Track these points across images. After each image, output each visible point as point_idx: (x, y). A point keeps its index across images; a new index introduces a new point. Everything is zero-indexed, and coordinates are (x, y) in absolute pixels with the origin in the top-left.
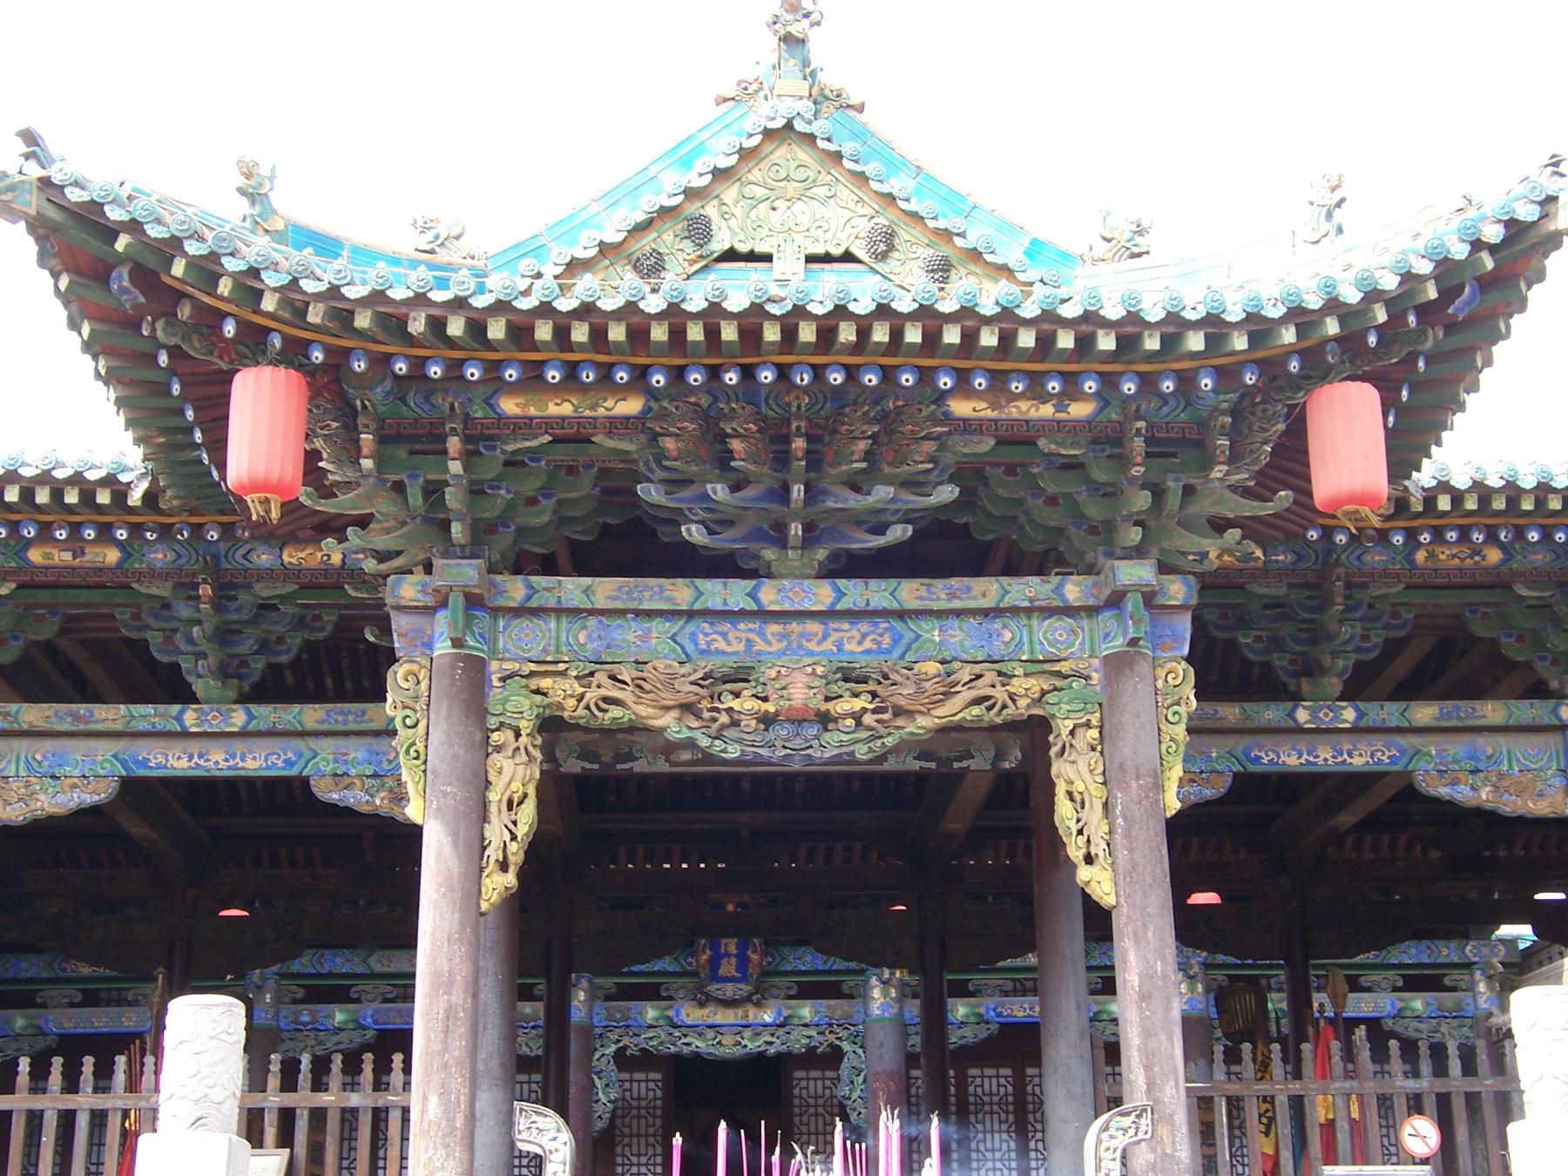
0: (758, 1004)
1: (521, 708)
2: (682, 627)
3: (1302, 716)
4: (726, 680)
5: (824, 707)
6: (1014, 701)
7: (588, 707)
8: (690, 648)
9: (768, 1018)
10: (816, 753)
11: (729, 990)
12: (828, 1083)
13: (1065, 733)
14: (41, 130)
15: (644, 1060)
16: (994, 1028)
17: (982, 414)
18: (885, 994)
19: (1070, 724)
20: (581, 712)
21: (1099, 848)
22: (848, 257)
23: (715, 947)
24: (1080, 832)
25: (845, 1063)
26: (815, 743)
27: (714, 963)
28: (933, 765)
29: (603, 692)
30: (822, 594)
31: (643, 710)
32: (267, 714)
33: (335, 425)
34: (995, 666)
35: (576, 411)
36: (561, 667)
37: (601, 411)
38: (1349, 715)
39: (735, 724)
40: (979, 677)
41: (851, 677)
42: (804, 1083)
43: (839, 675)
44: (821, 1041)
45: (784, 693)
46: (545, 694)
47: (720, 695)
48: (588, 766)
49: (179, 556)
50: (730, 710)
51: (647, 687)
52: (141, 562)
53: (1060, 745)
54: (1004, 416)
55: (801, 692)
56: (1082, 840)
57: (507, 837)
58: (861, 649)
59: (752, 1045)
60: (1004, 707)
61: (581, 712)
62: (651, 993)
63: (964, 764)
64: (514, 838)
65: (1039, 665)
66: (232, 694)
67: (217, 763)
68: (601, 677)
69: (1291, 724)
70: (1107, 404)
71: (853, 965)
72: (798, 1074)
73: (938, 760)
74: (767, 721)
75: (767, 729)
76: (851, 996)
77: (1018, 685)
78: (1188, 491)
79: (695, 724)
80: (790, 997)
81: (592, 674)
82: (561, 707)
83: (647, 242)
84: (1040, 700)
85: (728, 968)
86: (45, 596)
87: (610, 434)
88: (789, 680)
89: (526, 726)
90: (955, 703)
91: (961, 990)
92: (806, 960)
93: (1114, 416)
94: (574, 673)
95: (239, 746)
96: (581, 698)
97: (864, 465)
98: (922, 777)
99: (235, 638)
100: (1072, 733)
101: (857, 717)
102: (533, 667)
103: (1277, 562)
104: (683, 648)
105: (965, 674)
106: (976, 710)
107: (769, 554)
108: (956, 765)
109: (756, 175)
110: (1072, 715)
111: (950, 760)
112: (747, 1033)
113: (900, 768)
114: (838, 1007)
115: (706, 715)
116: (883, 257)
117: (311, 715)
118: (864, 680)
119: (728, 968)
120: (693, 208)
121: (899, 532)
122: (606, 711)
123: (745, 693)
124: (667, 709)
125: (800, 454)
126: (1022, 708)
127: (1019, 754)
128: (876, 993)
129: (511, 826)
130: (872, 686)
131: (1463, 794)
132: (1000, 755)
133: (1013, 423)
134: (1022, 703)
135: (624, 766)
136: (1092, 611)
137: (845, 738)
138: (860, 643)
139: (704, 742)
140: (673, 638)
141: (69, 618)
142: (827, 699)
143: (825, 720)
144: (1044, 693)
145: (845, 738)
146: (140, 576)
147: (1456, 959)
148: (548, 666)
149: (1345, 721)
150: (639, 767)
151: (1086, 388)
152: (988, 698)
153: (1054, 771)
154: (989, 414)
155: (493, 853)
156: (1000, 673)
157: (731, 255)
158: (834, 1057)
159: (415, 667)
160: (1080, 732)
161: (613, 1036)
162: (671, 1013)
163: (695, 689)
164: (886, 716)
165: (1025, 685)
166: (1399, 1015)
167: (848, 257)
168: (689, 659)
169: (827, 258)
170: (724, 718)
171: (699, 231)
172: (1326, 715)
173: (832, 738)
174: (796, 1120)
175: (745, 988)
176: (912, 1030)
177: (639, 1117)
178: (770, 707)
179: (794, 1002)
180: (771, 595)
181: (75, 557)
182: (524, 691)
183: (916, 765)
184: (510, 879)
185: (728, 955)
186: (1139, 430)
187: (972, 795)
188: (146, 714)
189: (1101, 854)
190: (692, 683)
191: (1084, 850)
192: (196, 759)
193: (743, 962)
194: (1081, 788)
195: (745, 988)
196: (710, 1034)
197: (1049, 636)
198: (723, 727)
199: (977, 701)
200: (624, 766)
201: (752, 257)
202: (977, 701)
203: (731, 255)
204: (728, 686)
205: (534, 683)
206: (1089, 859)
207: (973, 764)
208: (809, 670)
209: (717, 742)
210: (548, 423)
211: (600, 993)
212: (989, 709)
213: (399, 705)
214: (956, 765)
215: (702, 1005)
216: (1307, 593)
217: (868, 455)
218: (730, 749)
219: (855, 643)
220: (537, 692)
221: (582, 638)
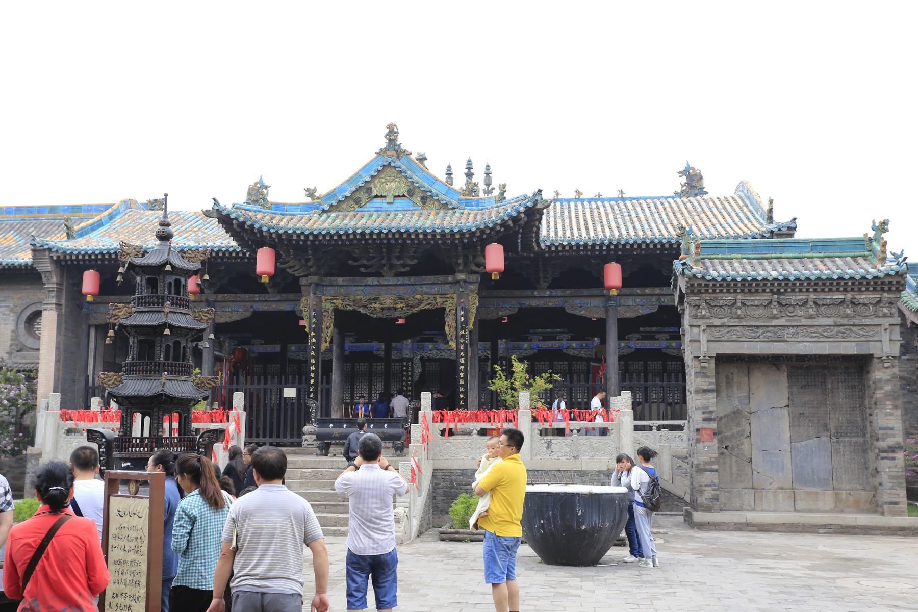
1: (328, 306)
3: (536, 293)
14: (217, 198)
16: (536, 351)
22: (404, 196)
30: (392, 281)
32: (284, 296)
38: (548, 293)
55: (388, 303)
62: (431, 340)
74: (383, 309)
83: (357, 195)
90: (422, 305)
95: (279, 303)
101: (402, 308)
109: (383, 176)
116: (411, 196)
117: (568, 292)
120: (368, 186)
121: (408, 269)
131: (577, 313)
143: (395, 309)
157: (377, 196)
166: (668, 347)
167: (404, 196)
169: (399, 196)
171: (369, 191)
180: (384, 281)
188: (256, 297)
201: (382, 196)
203: (377, 196)
219: (402, 291)
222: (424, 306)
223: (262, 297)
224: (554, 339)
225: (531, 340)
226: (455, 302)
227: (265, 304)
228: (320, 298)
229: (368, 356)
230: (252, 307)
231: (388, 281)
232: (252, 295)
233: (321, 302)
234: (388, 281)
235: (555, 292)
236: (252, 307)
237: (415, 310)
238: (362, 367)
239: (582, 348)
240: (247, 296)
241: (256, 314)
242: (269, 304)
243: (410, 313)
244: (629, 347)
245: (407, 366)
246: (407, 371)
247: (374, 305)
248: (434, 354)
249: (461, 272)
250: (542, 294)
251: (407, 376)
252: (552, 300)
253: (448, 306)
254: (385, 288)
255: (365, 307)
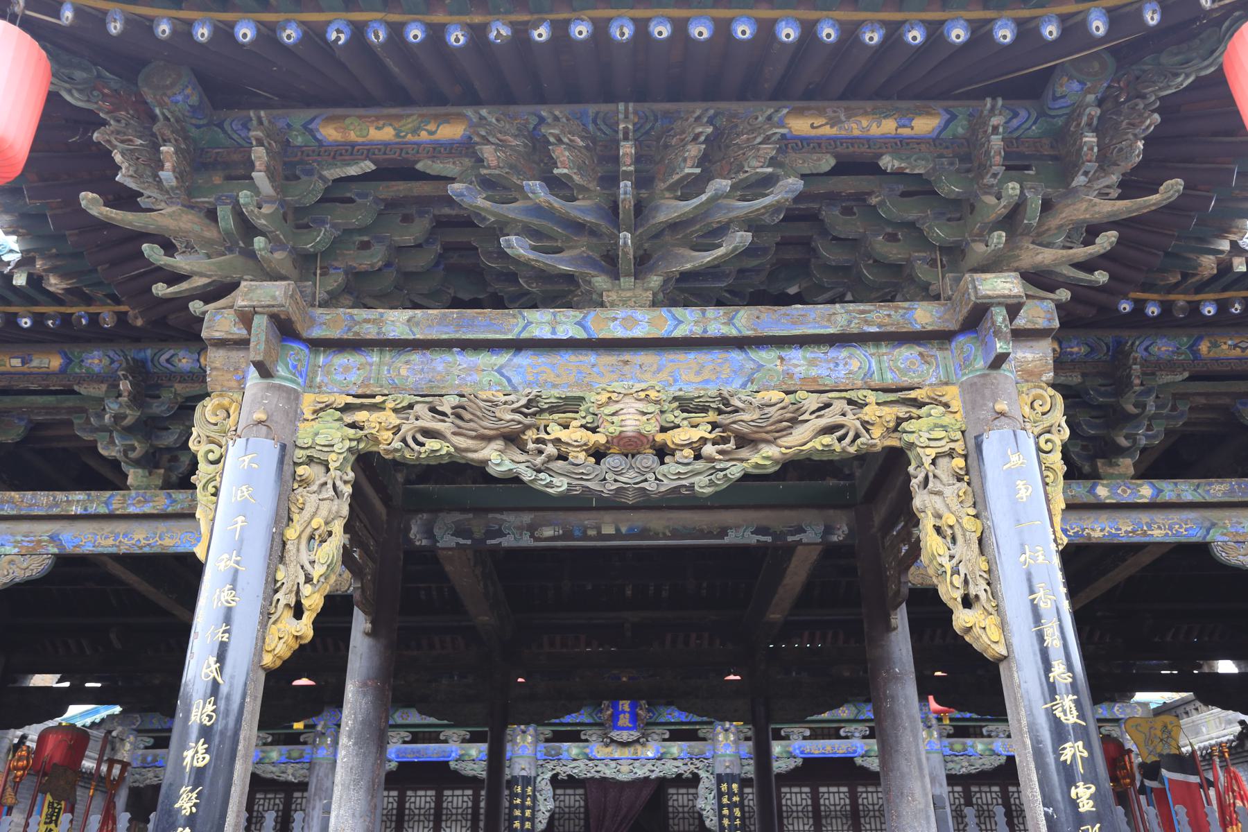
0: (643, 745)
1: (332, 436)
2: (510, 360)
4: (553, 410)
5: (660, 437)
6: (867, 430)
7: (404, 440)
9: (650, 754)
11: (625, 736)
12: (691, 797)
13: (927, 461)
15: (572, 782)
16: (799, 762)
17: (821, 132)
18: (727, 738)
19: (932, 453)
20: (397, 444)
21: (978, 588)
23: (615, 707)
24: (956, 571)
25: (701, 785)
26: (651, 476)
27: (615, 717)
28: (769, 539)
29: (420, 423)
30: (647, 323)
31: (462, 442)
33: (139, 142)
34: (844, 394)
35: (397, 135)
36: (379, 399)
39: (562, 457)
41: (686, 405)
42: (675, 797)
43: (676, 404)
44: (685, 770)
45: (615, 419)
46: (362, 428)
47: (546, 427)
48: (462, 541)
49: (113, 362)
50: (557, 441)
51: (467, 416)
53: (921, 477)
54: (843, 132)
56: (958, 581)
57: (302, 579)
58: (699, 379)
59: (641, 773)
60: (857, 436)
61: (397, 444)
62: (574, 737)
63: (797, 538)
64: (308, 580)
65: (896, 392)
68: (421, 409)
69: (1091, 500)
70: (953, 117)
71: (705, 719)
72: (672, 791)
75: (598, 463)
76: (704, 739)
77: (870, 413)
78: (1047, 206)
80: (664, 740)
81: (411, 406)
82: (376, 441)
84: (895, 430)
85: (624, 720)
91: (778, 736)
92: (674, 715)
93: (960, 130)
95: (161, 526)
96: (397, 430)
97: (698, 171)
98: (761, 549)
99: (165, 433)
100: (934, 463)
102: (350, 400)
103: (1071, 354)
104: (509, 380)
105: (813, 402)
106: (827, 439)
108: (790, 539)
110: (933, 444)
111: (783, 535)
112: (637, 764)
114: (696, 746)
115: (531, 446)
117: (1218, 489)
118: (705, 409)
119: (624, 720)
122: (422, 445)
123: (574, 423)
124: (489, 439)
125: (628, 161)
126: (877, 439)
127: (845, 528)
128: (721, 737)
129: (308, 566)
130: (712, 416)
132: (828, 530)
133: (853, 140)
134: (877, 432)
135: (493, 542)
136: (941, 337)
137: (682, 469)
138: (698, 373)
140: (499, 371)
141: (38, 426)
142: (663, 430)
144: (900, 421)
145: (682, 469)
146: (81, 380)
147: (1108, 716)
148: (366, 401)
149: (1143, 497)
150: (508, 542)
151: (953, 36)
152: (841, 426)
153: (917, 503)
154: (828, 131)
155: (284, 598)
156: (850, 402)
158: (695, 780)
159: (226, 401)
160: (943, 462)
161: (550, 766)
162: (587, 751)
164: (731, 445)
165: (879, 413)
168: (515, 390)
170: (550, 450)
172: (1124, 491)
173: (671, 467)
174: (671, 822)
175: (635, 734)
176: (745, 762)
177: (569, 819)
178: (601, 438)
179: (668, 743)
181: (23, 363)
183: (753, 539)
184: (305, 628)
185: (624, 712)
186: (995, 128)
187: (797, 574)
188: (77, 501)
189: (983, 596)
190: (514, 411)
191: (962, 591)
192: (121, 538)
193: (634, 717)
194: (952, 520)
195: (635, 734)
196: (613, 764)
197: (902, 363)
198: (550, 459)
200: (493, 542)
204: (556, 416)
205: (349, 419)
206: (967, 602)
207: (804, 537)
208: (642, 395)
209: (542, 475)
210: (368, 151)
211: (542, 737)
212: (840, 439)
213: (204, 439)
214: (790, 539)
215: (607, 745)
216: (1101, 381)
218: (556, 481)
220: (353, 426)
221: (404, 372)
223: (97, 501)
224: (435, 738)
225: (787, 738)
226: (955, 421)
227: (108, 527)
228: (294, 397)
229: (439, 776)
230: (53, 538)
231: (629, 322)
232: (61, 496)
235: (1172, 490)
236: (53, 538)
238: (421, 799)
239: (290, 760)
240: (42, 500)
241: (69, 566)
242: (121, 527)
243: (736, 471)
244: (994, 753)
245: (523, 796)
246: (523, 807)
247: (556, 432)
248: (581, 769)
249: (992, 265)
250: (1125, 495)
251: (731, 794)
252: (1160, 517)
253: (926, 435)
255: (513, 439)
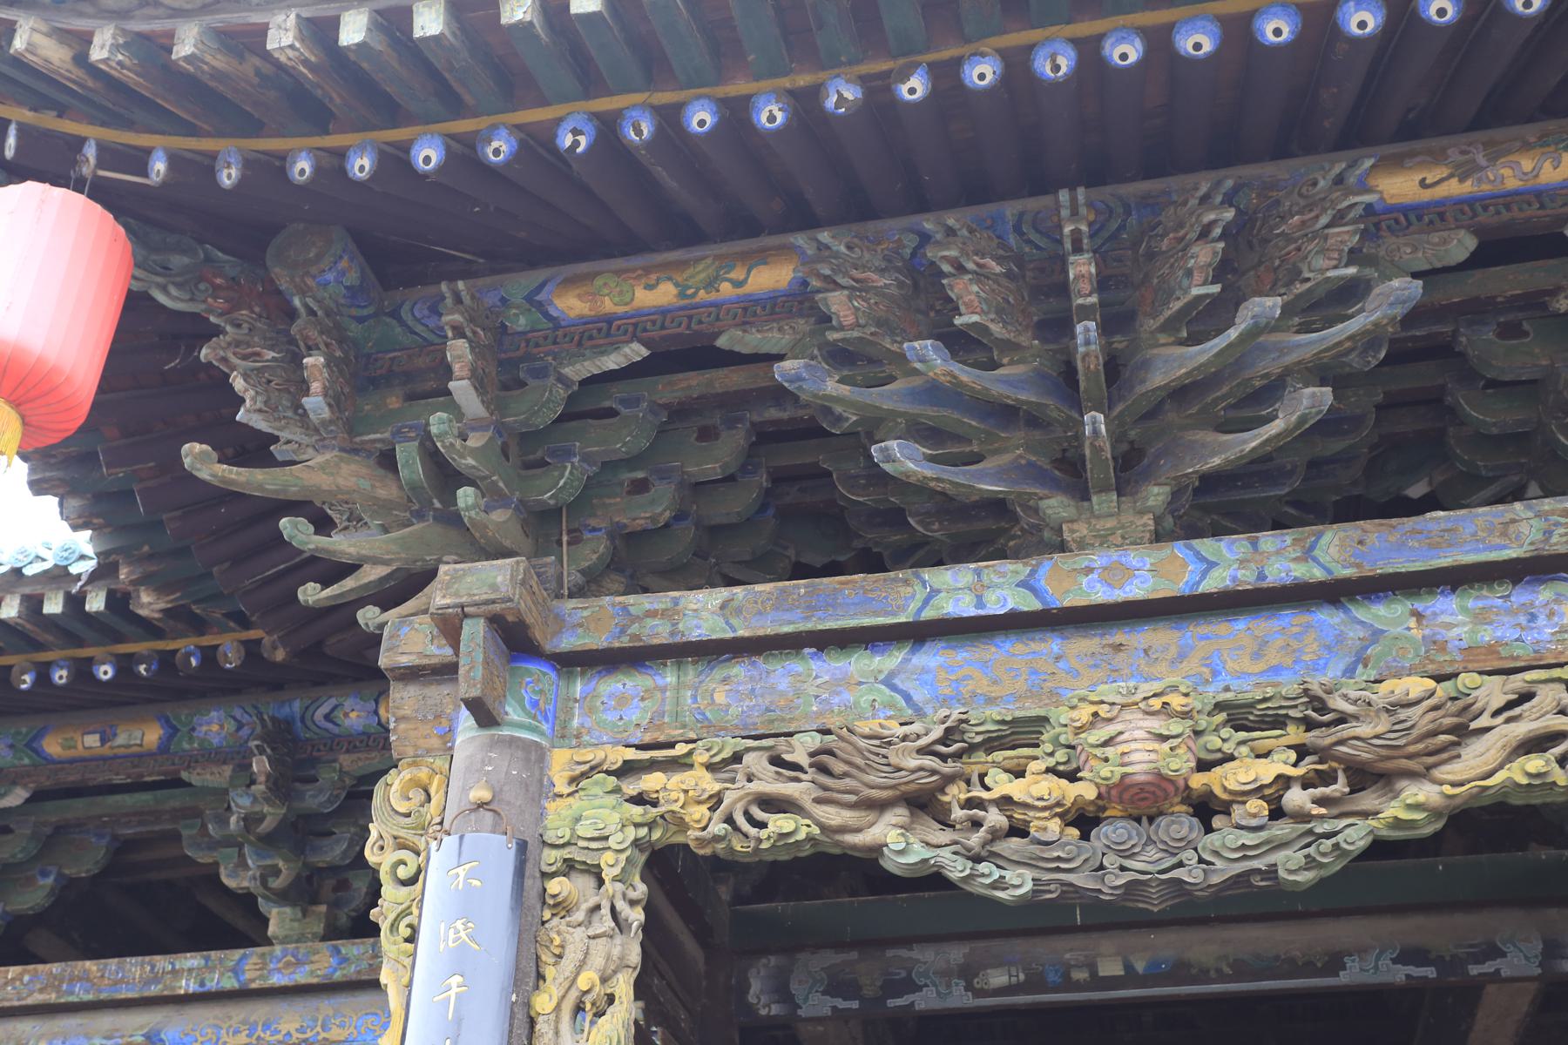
1: (604, 821)
5: (1198, 781)
7: (729, 820)
8: (919, 695)
10: (1191, 875)
17: (1441, 191)
20: (718, 828)
28: (1430, 972)
29: (755, 787)
33: (270, 354)
36: (681, 749)
37: (726, 289)
39: (1018, 831)
40: (1526, 697)
41: (1240, 716)
43: (1222, 717)
45: (1110, 752)
46: (655, 804)
47: (982, 776)
49: (240, 726)
50: (1006, 802)
51: (838, 767)
52: (191, 740)
54: (1486, 188)
55: (1140, 750)
61: (718, 828)
63: (1488, 967)
66: (319, 928)
67: (289, 1034)
73: (1437, 962)
74: (1084, 820)
75: (1085, 836)
79: (945, 836)
81: (737, 758)
82: (682, 826)
86: (78, 808)
87: (744, 325)
88: (1111, 729)
89: (610, 864)
94: (701, 757)
95: (325, 1006)
96: (716, 801)
98: (1413, 991)
101: (1273, 795)
102: (632, 754)
104: (908, 698)
105: (1493, 692)
107: (1056, 506)
108: (1474, 970)
113: (1370, 978)
115: (958, 813)
118: (1279, 722)
123: (1034, 766)
124: (880, 806)
125: (1086, 287)
135: (900, 1002)
137: (1249, 839)
139: (957, 869)
140: (888, 682)
142: (1203, 766)
145: (1249, 839)
150: (925, 1000)
154: (1455, 188)
159: (423, 774)
163: (929, 762)
168: (920, 713)
170: (995, 818)
173: (1225, 836)
181: (103, 741)
182: (612, 800)
183: (1399, 974)
190: (923, 751)
192: (259, 1032)
198: (996, 835)
199: (1537, 744)
200: (900, 1002)
202: (1537, 744)
204: (998, 756)
208: (1156, 703)
209: (984, 867)
210: (634, 326)
213: (389, 842)
217: (1222, 271)
219: (1245, 659)
220: (639, 800)
221: (720, 698)
222: (1484, 765)
228: (536, 756)
232: (162, 962)
233: (540, 791)
234: (1114, 573)
237: (1413, 803)
243: (1356, 836)
247: (1002, 784)
254: (1082, 646)
255: (923, 803)
